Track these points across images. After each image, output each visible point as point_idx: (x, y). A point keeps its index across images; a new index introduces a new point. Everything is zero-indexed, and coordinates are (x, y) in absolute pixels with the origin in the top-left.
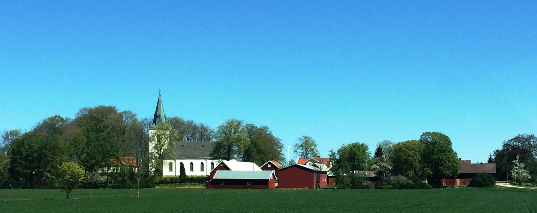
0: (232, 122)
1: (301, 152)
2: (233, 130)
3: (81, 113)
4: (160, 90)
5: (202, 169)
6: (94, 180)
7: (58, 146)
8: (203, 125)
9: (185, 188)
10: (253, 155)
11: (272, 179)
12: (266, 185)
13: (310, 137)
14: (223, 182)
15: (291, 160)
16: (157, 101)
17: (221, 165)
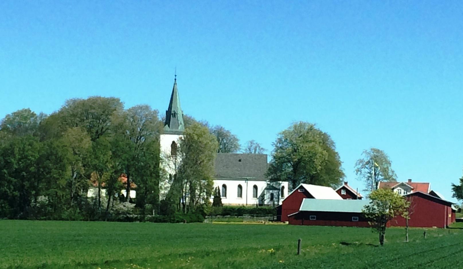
1: (368, 173)
4: (176, 76)
5: (240, 195)
13: (382, 151)
14: (315, 216)
16: (173, 87)
17: (299, 191)
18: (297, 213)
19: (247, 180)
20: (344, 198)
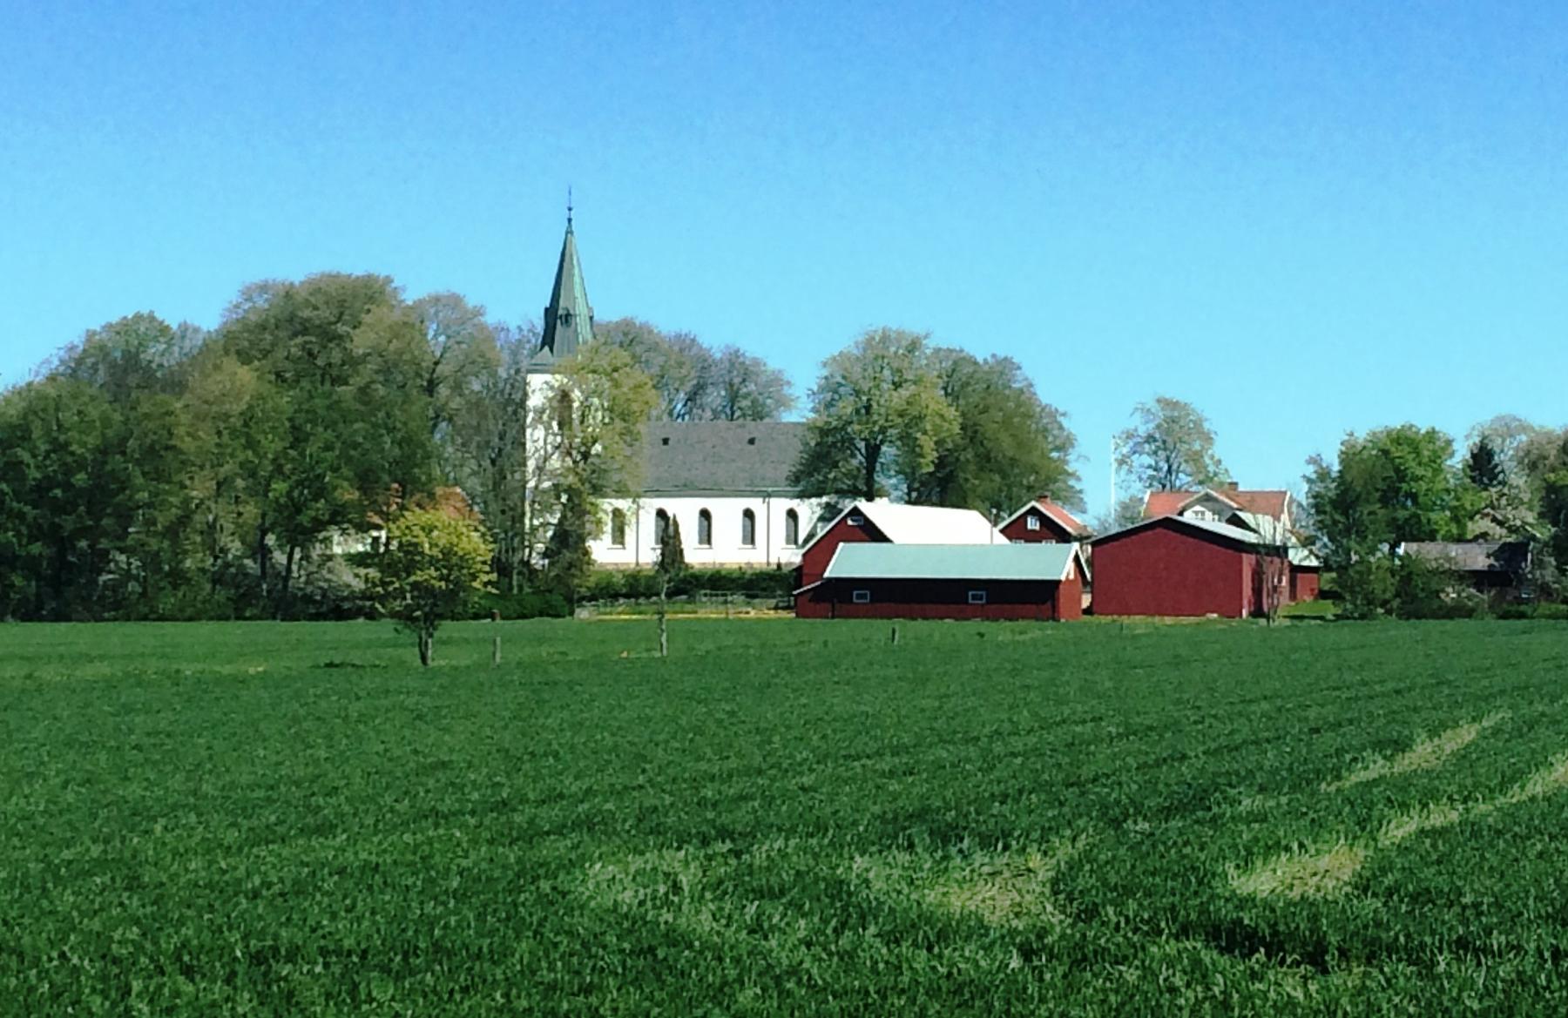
0: (885, 339)
1: (1150, 467)
2: (887, 372)
3: (247, 306)
4: (570, 209)
5: (750, 538)
6: (321, 584)
7: (173, 442)
8: (738, 351)
9: (698, 615)
10: (969, 478)
11: (1072, 577)
12: (1049, 604)
14: (984, 593)
15: (1131, 500)
17: (850, 522)
18: (818, 583)
19: (769, 496)
20: (1010, 538)
